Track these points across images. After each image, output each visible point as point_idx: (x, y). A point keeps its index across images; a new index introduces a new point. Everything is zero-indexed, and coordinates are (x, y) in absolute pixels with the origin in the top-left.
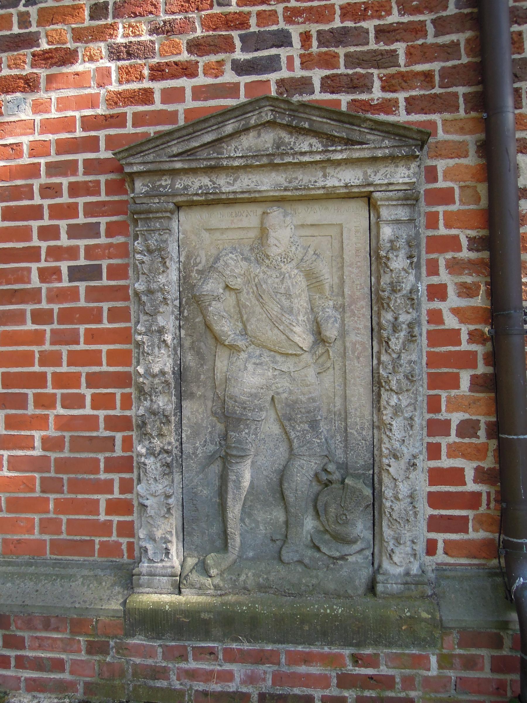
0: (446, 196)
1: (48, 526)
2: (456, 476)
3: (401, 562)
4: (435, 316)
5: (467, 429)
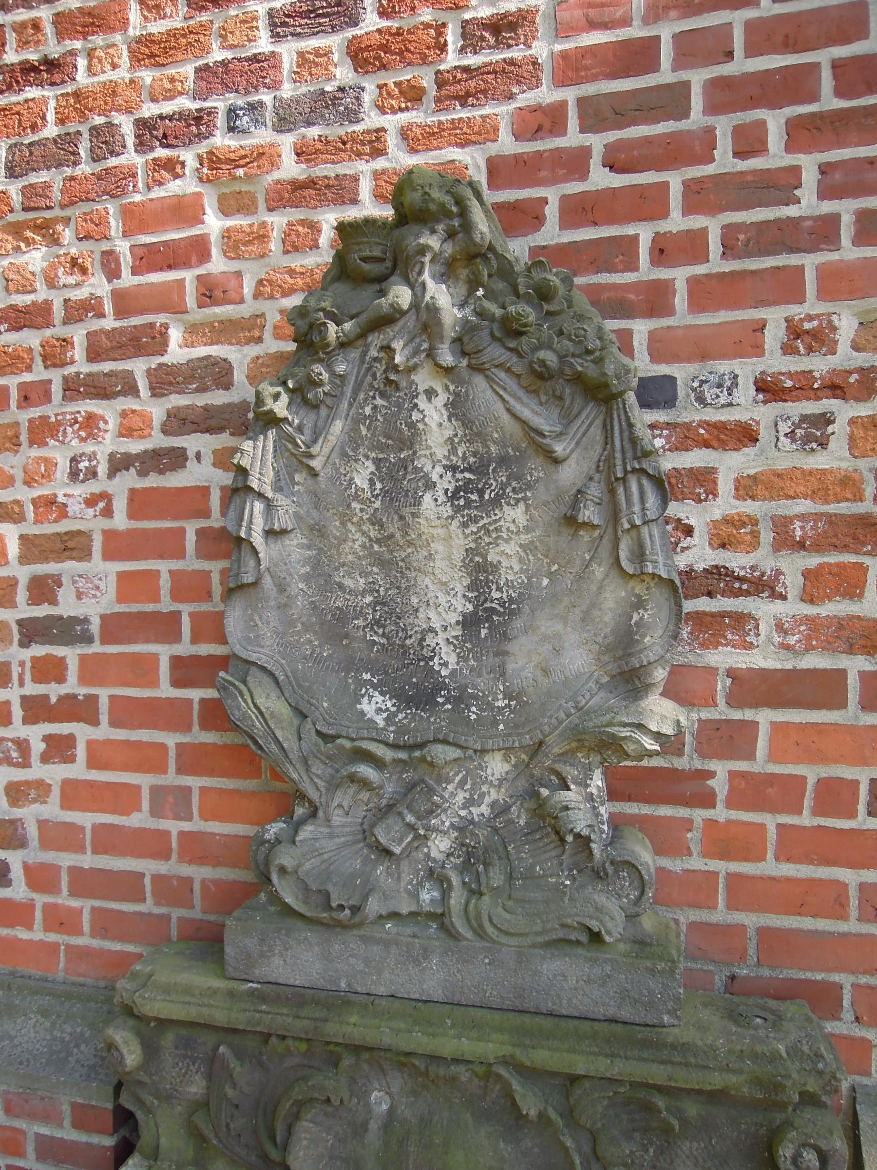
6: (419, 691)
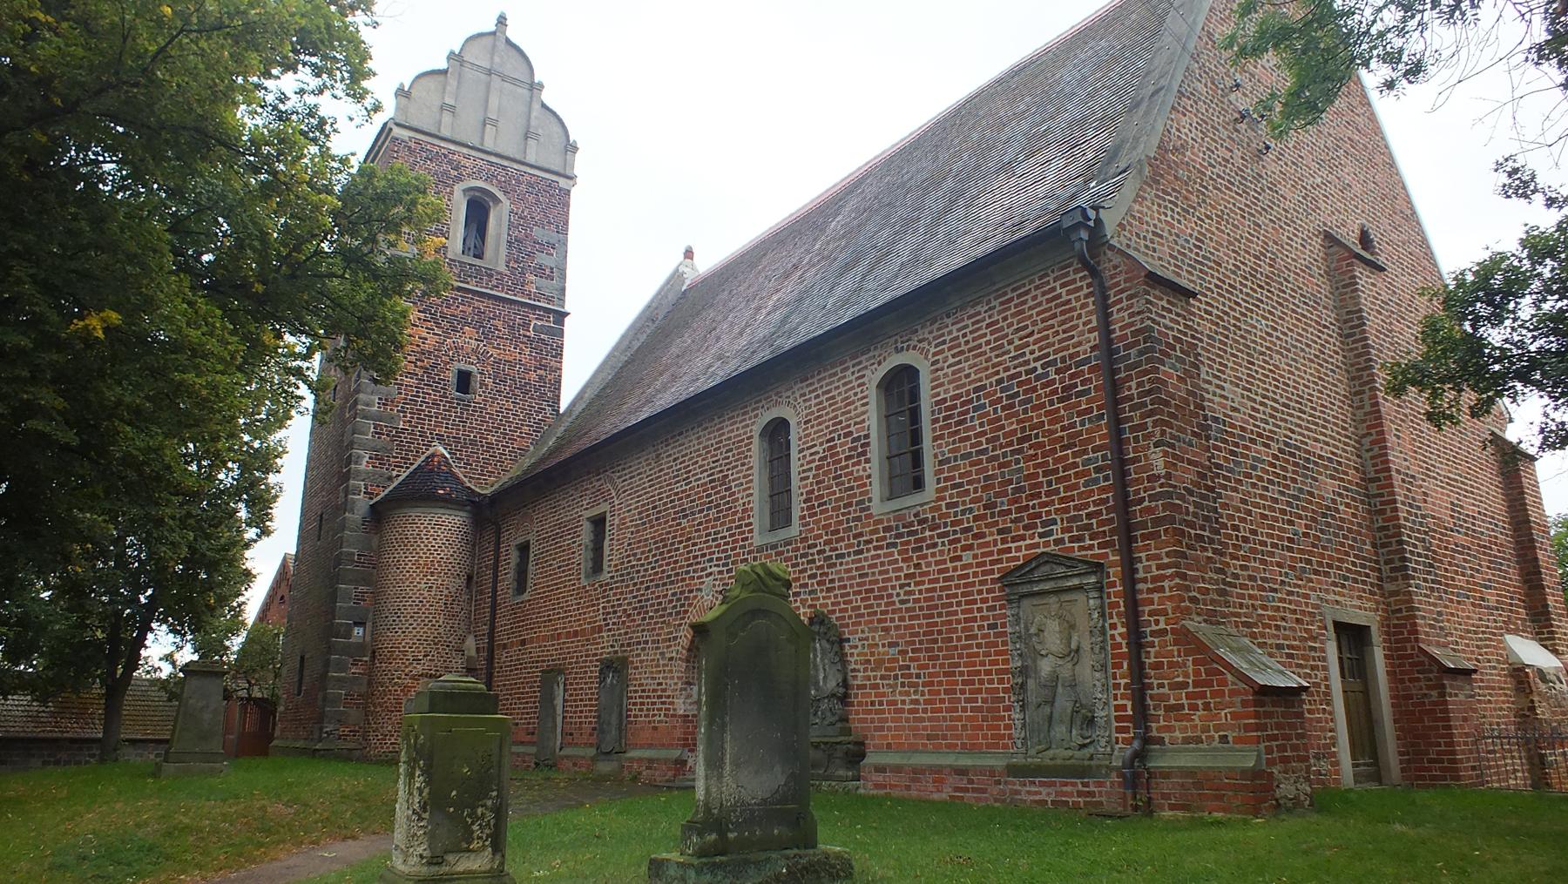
0: (1113, 584)
1: (985, 737)
2: (1124, 707)
4: (1113, 637)
5: (1126, 686)
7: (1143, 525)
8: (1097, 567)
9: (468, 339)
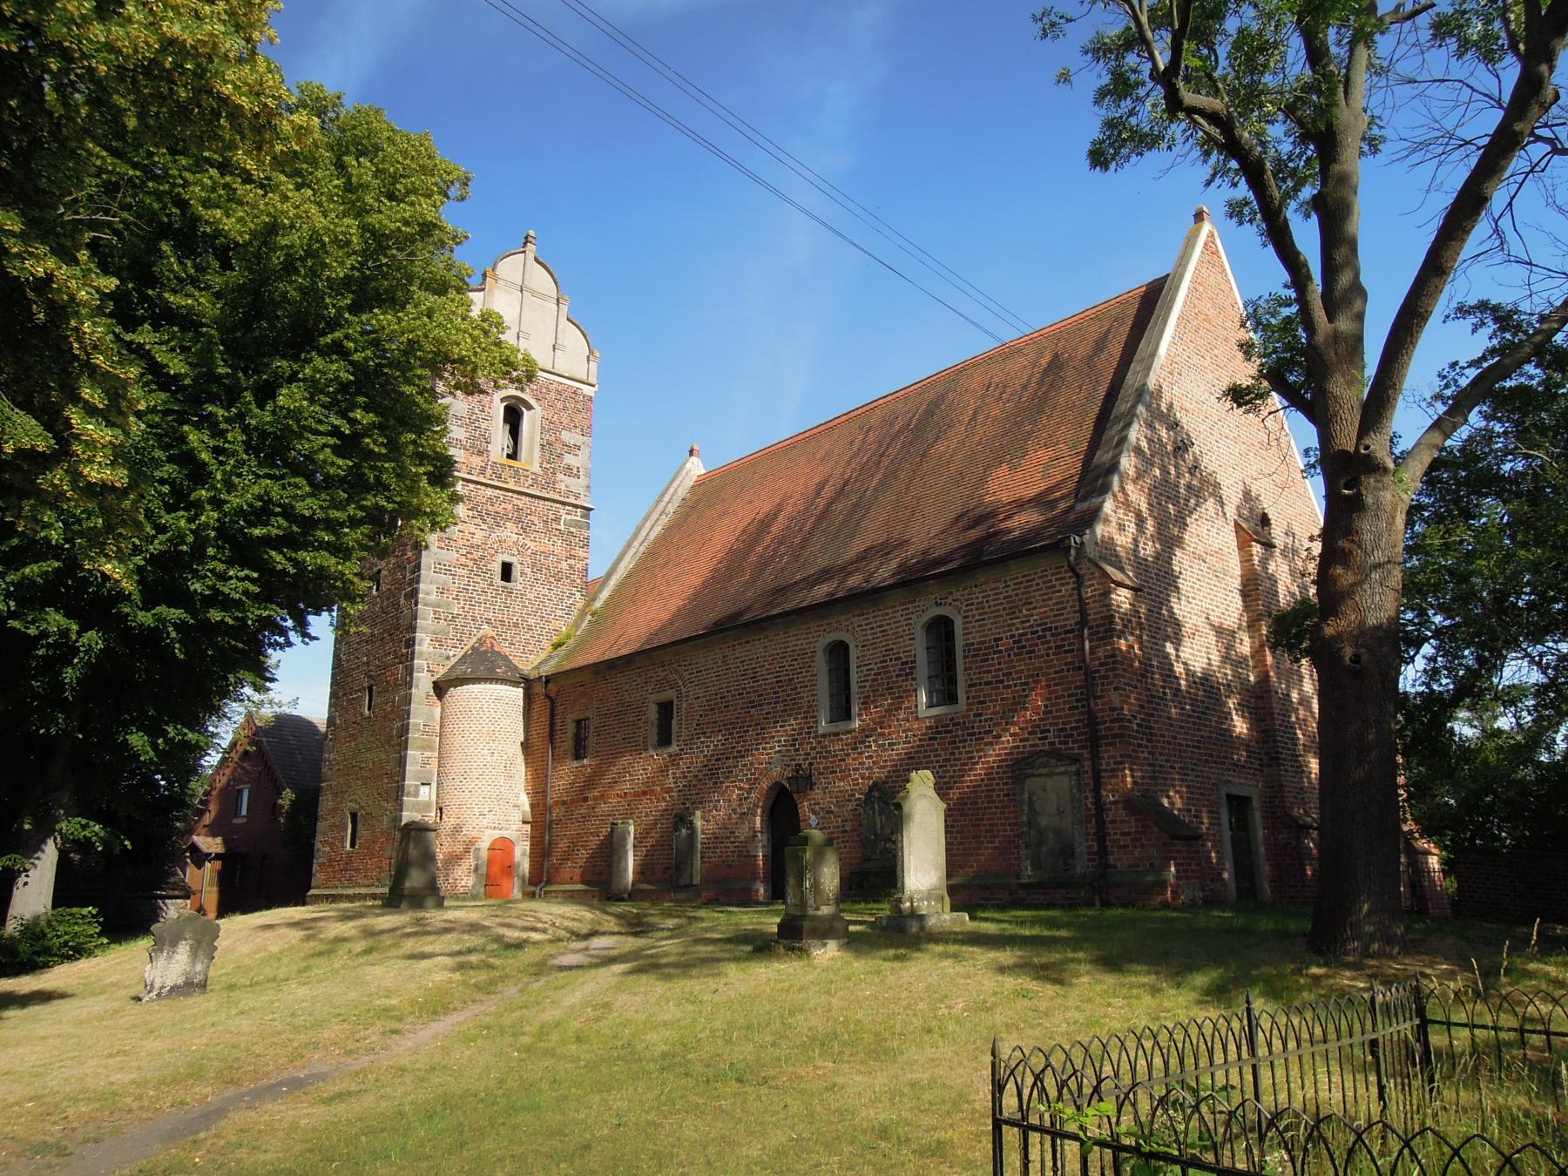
3: (1079, 870)
6: (876, 834)
7: (1106, 737)
8: (1075, 760)
9: (509, 532)
